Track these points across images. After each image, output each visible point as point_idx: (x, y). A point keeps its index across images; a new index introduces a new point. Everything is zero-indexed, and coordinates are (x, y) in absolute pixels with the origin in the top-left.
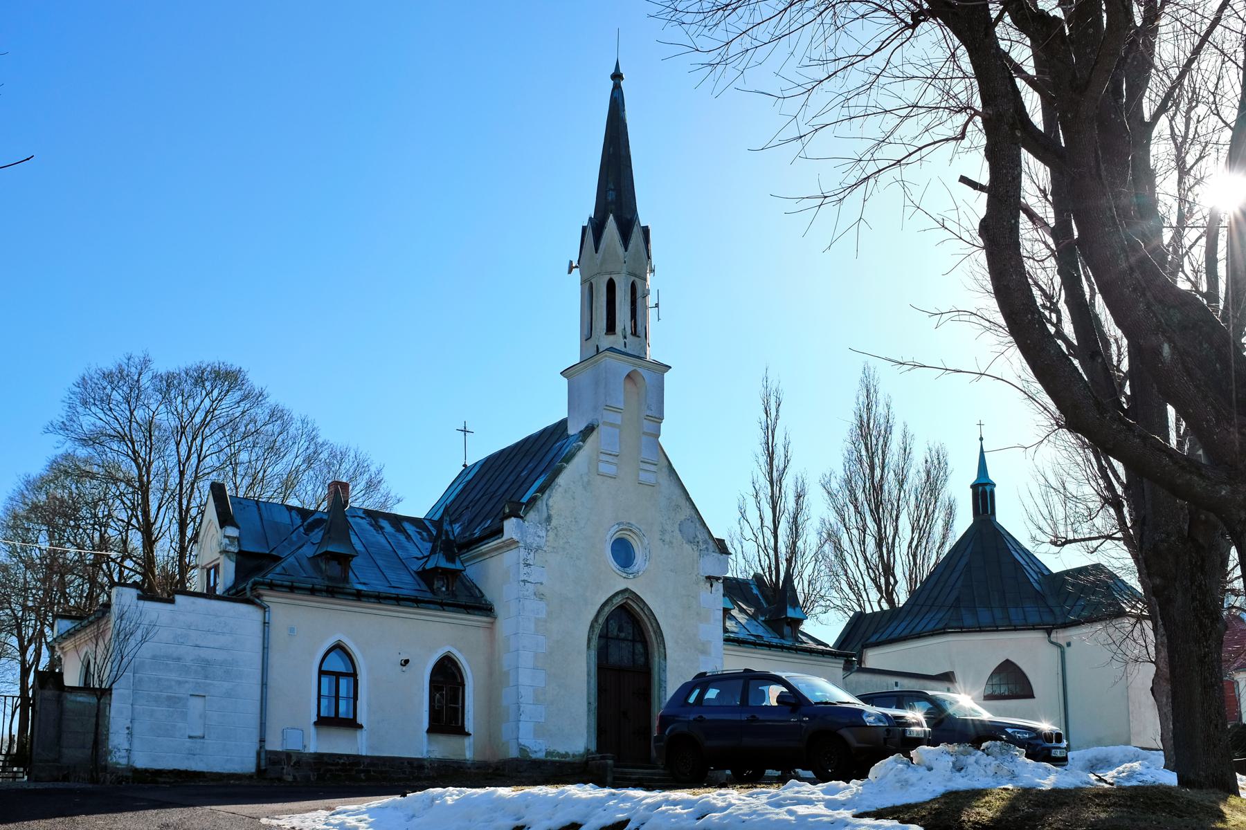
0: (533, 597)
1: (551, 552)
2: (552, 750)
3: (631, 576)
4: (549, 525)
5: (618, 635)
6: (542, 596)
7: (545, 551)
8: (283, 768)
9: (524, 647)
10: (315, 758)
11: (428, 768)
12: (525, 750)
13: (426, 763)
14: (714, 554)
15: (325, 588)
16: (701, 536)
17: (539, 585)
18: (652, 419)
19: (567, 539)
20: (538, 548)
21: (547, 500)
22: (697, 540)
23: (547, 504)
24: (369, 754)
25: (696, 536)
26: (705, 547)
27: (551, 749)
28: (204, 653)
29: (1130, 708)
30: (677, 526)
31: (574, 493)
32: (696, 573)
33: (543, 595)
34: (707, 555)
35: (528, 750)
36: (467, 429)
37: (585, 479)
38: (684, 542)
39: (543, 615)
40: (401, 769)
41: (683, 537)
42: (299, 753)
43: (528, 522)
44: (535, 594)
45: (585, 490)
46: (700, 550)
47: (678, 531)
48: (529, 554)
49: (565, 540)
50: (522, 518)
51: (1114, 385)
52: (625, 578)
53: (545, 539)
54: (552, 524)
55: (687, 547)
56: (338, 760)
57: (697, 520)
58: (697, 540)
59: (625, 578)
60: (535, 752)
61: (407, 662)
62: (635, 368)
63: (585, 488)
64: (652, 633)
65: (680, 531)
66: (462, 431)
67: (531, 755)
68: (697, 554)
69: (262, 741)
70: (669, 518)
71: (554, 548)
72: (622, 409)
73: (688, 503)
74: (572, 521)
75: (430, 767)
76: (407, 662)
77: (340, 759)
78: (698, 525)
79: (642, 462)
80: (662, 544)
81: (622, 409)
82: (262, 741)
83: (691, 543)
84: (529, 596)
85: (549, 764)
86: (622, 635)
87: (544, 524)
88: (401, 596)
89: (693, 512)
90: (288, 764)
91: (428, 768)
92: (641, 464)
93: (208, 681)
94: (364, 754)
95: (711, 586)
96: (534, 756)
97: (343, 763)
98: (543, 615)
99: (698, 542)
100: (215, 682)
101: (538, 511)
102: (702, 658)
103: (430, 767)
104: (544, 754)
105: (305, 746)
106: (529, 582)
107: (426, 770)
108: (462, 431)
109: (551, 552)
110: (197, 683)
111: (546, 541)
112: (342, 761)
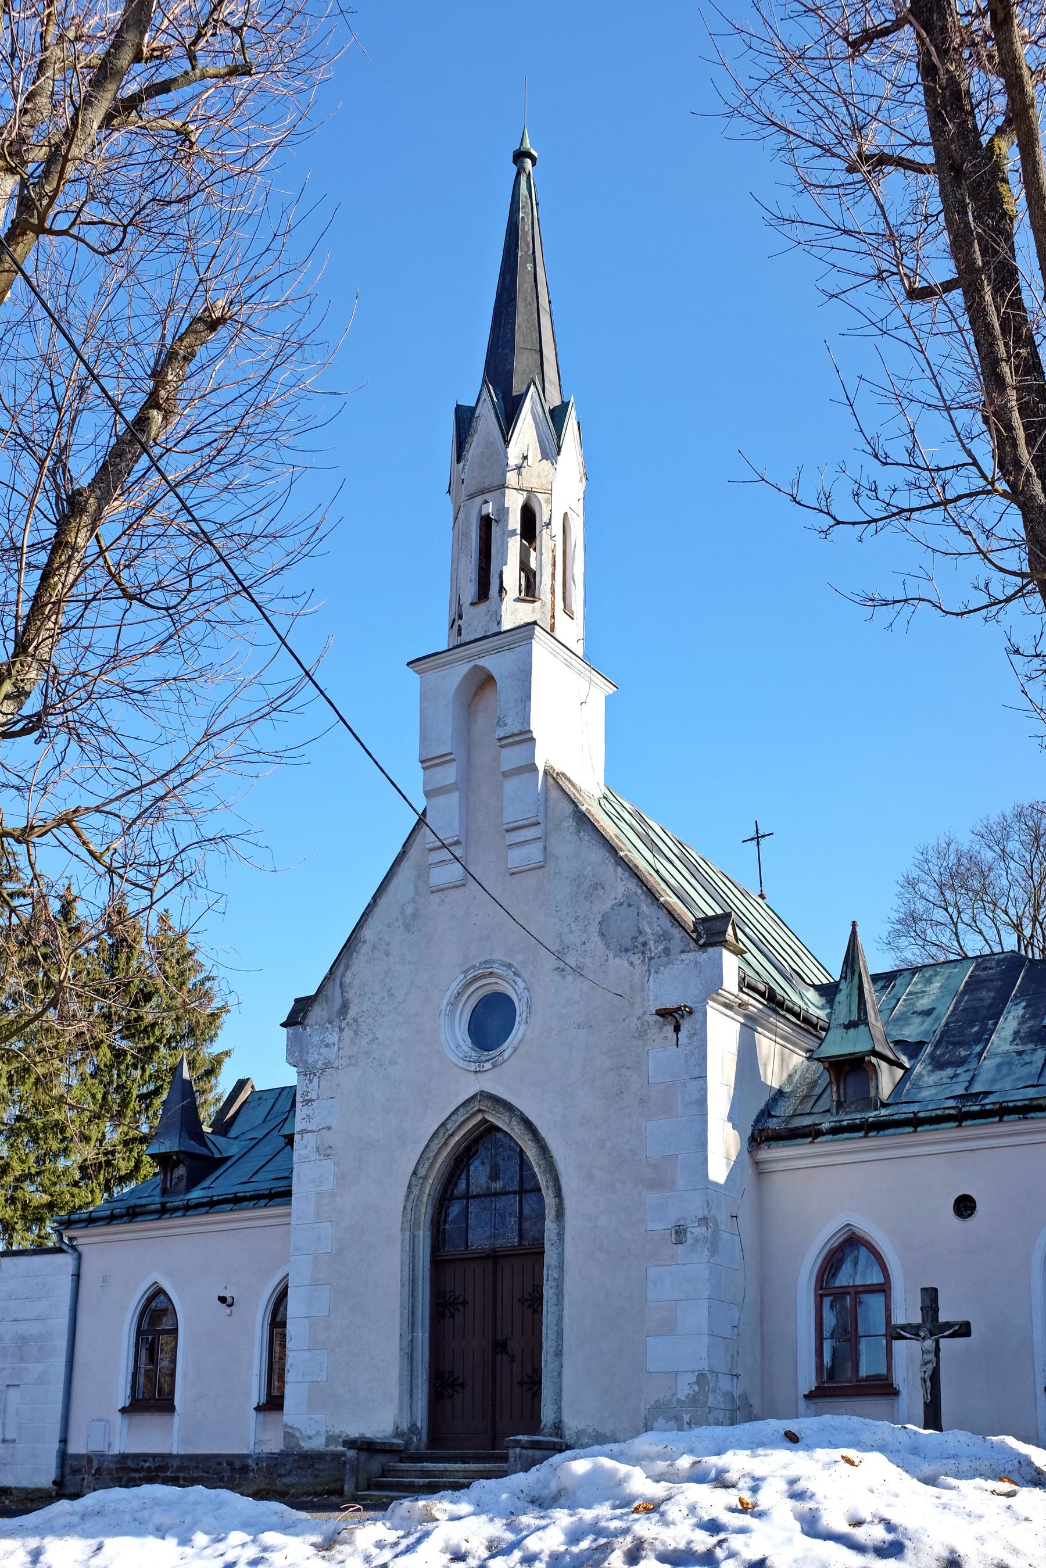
0: (314, 1156)
1: (347, 1066)
2: (337, 1432)
3: (488, 1066)
4: (345, 1019)
5: (488, 1187)
6: (329, 1151)
7: (337, 1068)
8: (83, 1479)
9: (297, 1249)
10: (118, 1462)
11: (253, 1471)
12: (293, 1436)
13: (250, 1462)
14: (684, 956)
15: (158, 1206)
16: (653, 924)
17: (325, 1131)
18: (510, 740)
19: (375, 1034)
20: (328, 1065)
21: (343, 975)
22: (641, 939)
23: (341, 984)
24: (182, 1452)
25: (640, 932)
26: (661, 947)
27: (336, 1431)
28: (23, 1328)
29: (470, 1237)
30: (594, 929)
31: (388, 944)
32: (640, 1013)
33: (330, 1147)
34: (666, 965)
35: (298, 1435)
36: (754, 835)
37: (409, 911)
38: (611, 955)
39: (328, 1186)
40: (217, 1473)
41: (608, 946)
42: (102, 1456)
43: (311, 1026)
44: (318, 1150)
45: (409, 931)
46: (650, 959)
47: (596, 938)
48: (311, 1081)
49: (370, 1036)
50: (301, 1023)
51: (142, 38)
52: (476, 1072)
53: (336, 1047)
54: (349, 1016)
55: (620, 963)
56: (142, 1463)
57: (642, 897)
58: (641, 939)
59: (476, 1072)
60: (310, 1438)
61: (222, 1300)
62: (472, 664)
63: (407, 928)
64: (431, 1181)
65: (602, 935)
66: (758, 843)
67: (302, 1444)
68: (641, 969)
69: (64, 1441)
70: (577, 918)
71: (351, 1057)
72: (451, 754)
73: (619, 869)
74: (383, 998)
75: (255, 1467)
76: (222, 1300)
77: (145, 1461)
78: (644, 908)
79: (507, 831)
80: (559, 978)
81: (451, 754)
82: (64, 1441)
83: (627, 950)
84: (308, 1157)
85: (328, 1458)
86: (498, 1185)
87: (336, 1022)
88: (215, 1199)
89: (632, 885)
90: (89, 1473)
91: (253, 1471)
92: (508, 835)
93: (23, 1365)
94: (175, 1452)
95: (677, 1029)
96: (307, 1446)
97: (149, 1467)
98: (328, 1186)
99: (644, 944)
100: (29, 1365)
101: (327, 1002)
102: (651, 1198)
103: (255, 1467)
104: (324, 1440)
105: (110, 1445)
106: (309, 1131)
107: (251, 1474)
108: (758, 843)
109: (347, 1066)
110: (14, 1369)
111: (339, 1049)
112: (148, 1464)
